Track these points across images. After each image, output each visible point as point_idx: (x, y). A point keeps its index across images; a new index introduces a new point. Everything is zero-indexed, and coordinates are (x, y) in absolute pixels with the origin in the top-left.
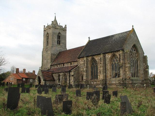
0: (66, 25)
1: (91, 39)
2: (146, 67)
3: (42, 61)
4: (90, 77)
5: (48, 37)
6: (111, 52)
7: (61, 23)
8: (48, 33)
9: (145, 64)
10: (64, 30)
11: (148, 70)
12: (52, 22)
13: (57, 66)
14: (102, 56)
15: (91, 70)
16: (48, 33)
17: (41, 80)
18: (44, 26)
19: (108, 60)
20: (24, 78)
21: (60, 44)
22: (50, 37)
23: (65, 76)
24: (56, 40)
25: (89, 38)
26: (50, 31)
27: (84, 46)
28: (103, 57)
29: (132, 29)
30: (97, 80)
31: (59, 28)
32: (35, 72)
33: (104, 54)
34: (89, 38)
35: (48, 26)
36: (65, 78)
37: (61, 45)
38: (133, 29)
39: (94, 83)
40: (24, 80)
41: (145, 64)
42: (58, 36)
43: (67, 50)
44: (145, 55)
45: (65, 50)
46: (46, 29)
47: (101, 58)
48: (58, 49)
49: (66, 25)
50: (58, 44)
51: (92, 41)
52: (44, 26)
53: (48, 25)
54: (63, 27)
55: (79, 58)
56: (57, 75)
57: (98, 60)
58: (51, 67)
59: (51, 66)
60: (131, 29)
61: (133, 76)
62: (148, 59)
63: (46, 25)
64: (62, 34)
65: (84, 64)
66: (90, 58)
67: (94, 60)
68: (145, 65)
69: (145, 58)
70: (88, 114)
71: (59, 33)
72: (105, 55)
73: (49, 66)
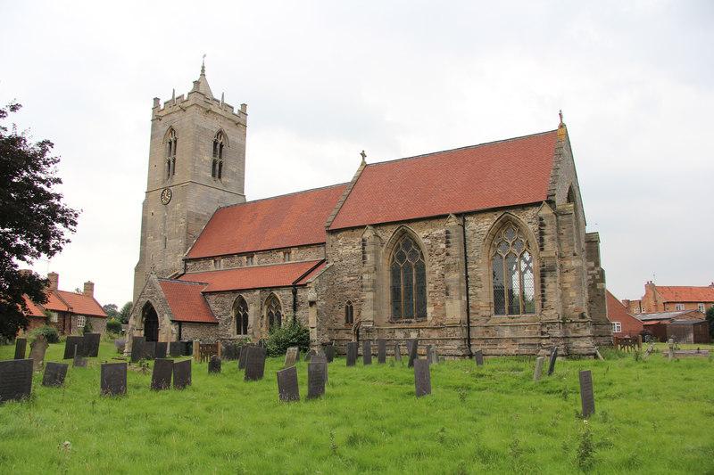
0: (244, 106)
1: (369, 161)
2: (598, 277)
4: (387, 312)
5: (172, 146)
7: (222, 88)
8: (172, 130)
9: (592, 264)
10: (239, 121)
13: (215, 262)
15: (393, 281)
16: (172, 130)
17: (157, 323)
18: (156, 100)
20: (54, 311)
21: (220, 177)
22: (184, 147)
23: (270, 306)
24: (208, 157)
25: (363, 155)
26: (183, 122)
27: (348, 183)
30: (421, 325)
31: (219, 111)
32: (92, 290)
33: (458, 215)
34: (363, 155)
36: (270, 314)
37: (223, 179)
38: (562, 126)
39: (407, 335)
40: (55, 318)
41: (592, 264)
42: (215, 144)
43: (245, 203)
44: (589, 230)
45: (240, 200)
46: (164, 113)
47: (447, 232)
48: (201, 199)
49: (244, 106)
50: (214, 175)
51: (379, 166)
52: (156, 100)
53: (176, 96)
57: (427, 241)
58: (186, 269)
59: (186, 261)
60: (553, 125)
62: (602, 247)
64: (231, 138)
65: (364, 258)
68: (593, 269)
69: (592, 243)
70: (4, 458)
71: (220, 133)
72: (464, 221)
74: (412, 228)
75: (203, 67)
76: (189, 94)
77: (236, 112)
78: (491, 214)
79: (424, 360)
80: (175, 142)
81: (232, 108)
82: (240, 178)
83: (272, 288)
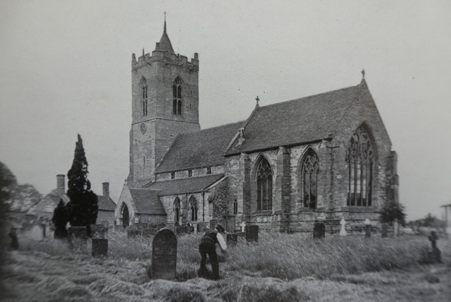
0: (196, 55)
1: (261, 105)
3: (169, 37)
5: (145, 89)
6: (303, 144)
11: (396, 186)
12: (158, 44)
14: (280, 152)
18: (134, 55)
19: (294, 163)
25: (257, 99)
28: (285, 155)
29: (362, 81)
34: (257, 99)
35: (144, 56)
38: (363, 81)
42: (174, 87)
47: (273, 160)
49: (196, 55)
51: (267, 108)
52: (134, 55)
53: (145, 53)
54: (189, 60)
55: (227, 156)
56: (172, 200)
59: (156, 174)
60: (356, 82)
61: (367, 203)
63: (139, 55)
64: (186, 81)
66: (254, 158)
67: (263, 161)
71: (178, 79)
73: (150, 174)
74: (267, 155)
75: (165, 22)
76: (153, 52)
77: (189, 60)
78: (301, 147)
79: (93, 212)
80: (147, 88)
81: (186, 58)
82: (195, 109)
83: (178, 194)
